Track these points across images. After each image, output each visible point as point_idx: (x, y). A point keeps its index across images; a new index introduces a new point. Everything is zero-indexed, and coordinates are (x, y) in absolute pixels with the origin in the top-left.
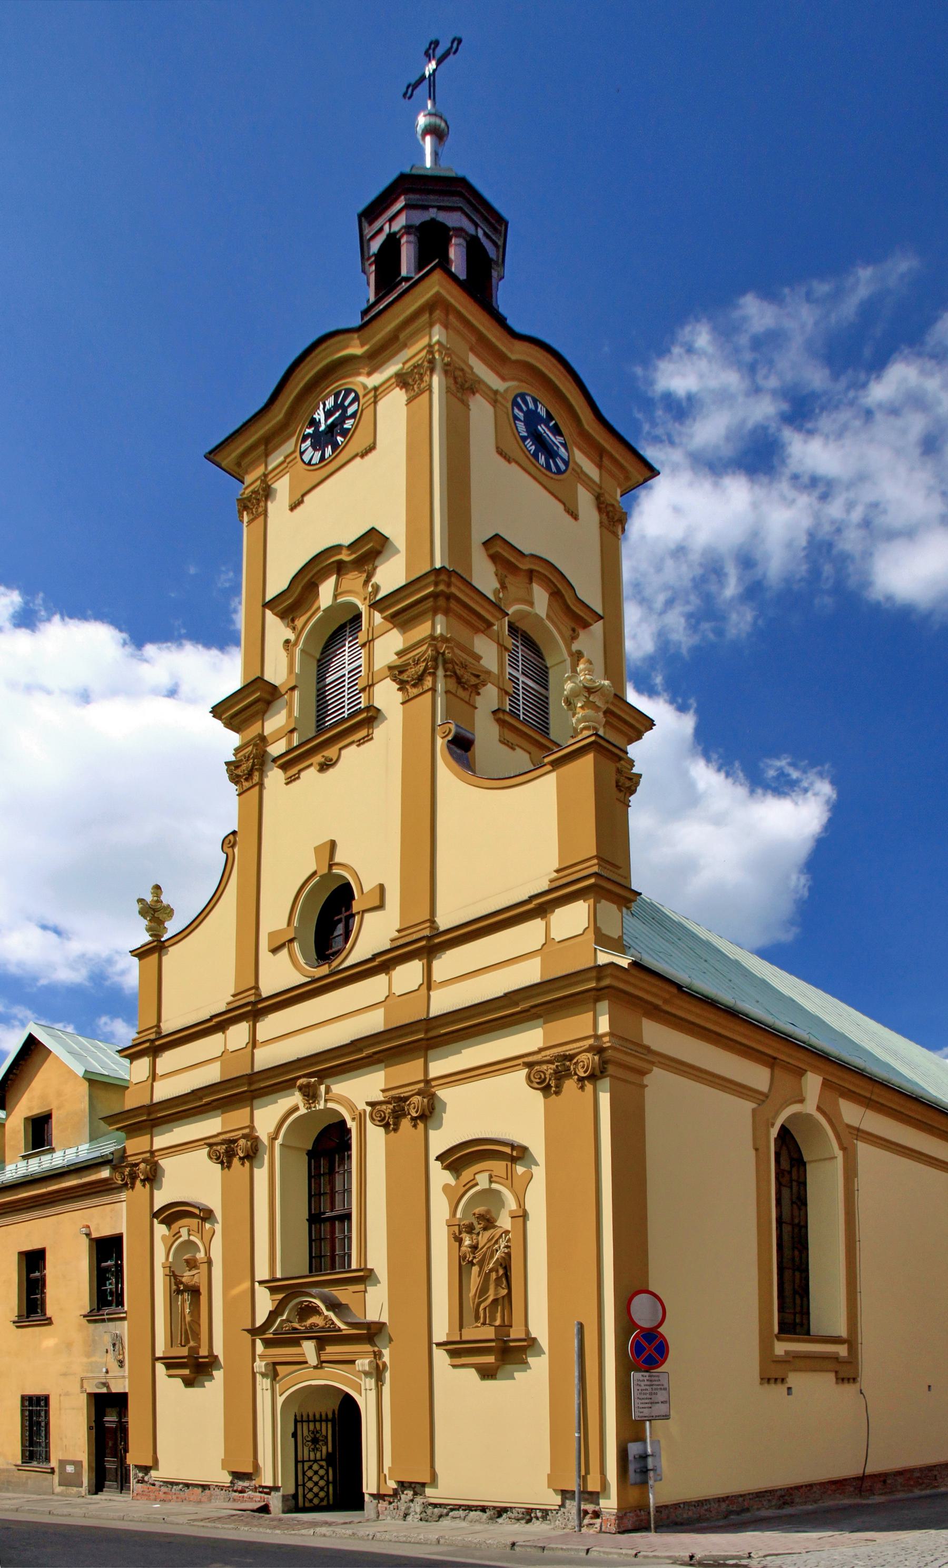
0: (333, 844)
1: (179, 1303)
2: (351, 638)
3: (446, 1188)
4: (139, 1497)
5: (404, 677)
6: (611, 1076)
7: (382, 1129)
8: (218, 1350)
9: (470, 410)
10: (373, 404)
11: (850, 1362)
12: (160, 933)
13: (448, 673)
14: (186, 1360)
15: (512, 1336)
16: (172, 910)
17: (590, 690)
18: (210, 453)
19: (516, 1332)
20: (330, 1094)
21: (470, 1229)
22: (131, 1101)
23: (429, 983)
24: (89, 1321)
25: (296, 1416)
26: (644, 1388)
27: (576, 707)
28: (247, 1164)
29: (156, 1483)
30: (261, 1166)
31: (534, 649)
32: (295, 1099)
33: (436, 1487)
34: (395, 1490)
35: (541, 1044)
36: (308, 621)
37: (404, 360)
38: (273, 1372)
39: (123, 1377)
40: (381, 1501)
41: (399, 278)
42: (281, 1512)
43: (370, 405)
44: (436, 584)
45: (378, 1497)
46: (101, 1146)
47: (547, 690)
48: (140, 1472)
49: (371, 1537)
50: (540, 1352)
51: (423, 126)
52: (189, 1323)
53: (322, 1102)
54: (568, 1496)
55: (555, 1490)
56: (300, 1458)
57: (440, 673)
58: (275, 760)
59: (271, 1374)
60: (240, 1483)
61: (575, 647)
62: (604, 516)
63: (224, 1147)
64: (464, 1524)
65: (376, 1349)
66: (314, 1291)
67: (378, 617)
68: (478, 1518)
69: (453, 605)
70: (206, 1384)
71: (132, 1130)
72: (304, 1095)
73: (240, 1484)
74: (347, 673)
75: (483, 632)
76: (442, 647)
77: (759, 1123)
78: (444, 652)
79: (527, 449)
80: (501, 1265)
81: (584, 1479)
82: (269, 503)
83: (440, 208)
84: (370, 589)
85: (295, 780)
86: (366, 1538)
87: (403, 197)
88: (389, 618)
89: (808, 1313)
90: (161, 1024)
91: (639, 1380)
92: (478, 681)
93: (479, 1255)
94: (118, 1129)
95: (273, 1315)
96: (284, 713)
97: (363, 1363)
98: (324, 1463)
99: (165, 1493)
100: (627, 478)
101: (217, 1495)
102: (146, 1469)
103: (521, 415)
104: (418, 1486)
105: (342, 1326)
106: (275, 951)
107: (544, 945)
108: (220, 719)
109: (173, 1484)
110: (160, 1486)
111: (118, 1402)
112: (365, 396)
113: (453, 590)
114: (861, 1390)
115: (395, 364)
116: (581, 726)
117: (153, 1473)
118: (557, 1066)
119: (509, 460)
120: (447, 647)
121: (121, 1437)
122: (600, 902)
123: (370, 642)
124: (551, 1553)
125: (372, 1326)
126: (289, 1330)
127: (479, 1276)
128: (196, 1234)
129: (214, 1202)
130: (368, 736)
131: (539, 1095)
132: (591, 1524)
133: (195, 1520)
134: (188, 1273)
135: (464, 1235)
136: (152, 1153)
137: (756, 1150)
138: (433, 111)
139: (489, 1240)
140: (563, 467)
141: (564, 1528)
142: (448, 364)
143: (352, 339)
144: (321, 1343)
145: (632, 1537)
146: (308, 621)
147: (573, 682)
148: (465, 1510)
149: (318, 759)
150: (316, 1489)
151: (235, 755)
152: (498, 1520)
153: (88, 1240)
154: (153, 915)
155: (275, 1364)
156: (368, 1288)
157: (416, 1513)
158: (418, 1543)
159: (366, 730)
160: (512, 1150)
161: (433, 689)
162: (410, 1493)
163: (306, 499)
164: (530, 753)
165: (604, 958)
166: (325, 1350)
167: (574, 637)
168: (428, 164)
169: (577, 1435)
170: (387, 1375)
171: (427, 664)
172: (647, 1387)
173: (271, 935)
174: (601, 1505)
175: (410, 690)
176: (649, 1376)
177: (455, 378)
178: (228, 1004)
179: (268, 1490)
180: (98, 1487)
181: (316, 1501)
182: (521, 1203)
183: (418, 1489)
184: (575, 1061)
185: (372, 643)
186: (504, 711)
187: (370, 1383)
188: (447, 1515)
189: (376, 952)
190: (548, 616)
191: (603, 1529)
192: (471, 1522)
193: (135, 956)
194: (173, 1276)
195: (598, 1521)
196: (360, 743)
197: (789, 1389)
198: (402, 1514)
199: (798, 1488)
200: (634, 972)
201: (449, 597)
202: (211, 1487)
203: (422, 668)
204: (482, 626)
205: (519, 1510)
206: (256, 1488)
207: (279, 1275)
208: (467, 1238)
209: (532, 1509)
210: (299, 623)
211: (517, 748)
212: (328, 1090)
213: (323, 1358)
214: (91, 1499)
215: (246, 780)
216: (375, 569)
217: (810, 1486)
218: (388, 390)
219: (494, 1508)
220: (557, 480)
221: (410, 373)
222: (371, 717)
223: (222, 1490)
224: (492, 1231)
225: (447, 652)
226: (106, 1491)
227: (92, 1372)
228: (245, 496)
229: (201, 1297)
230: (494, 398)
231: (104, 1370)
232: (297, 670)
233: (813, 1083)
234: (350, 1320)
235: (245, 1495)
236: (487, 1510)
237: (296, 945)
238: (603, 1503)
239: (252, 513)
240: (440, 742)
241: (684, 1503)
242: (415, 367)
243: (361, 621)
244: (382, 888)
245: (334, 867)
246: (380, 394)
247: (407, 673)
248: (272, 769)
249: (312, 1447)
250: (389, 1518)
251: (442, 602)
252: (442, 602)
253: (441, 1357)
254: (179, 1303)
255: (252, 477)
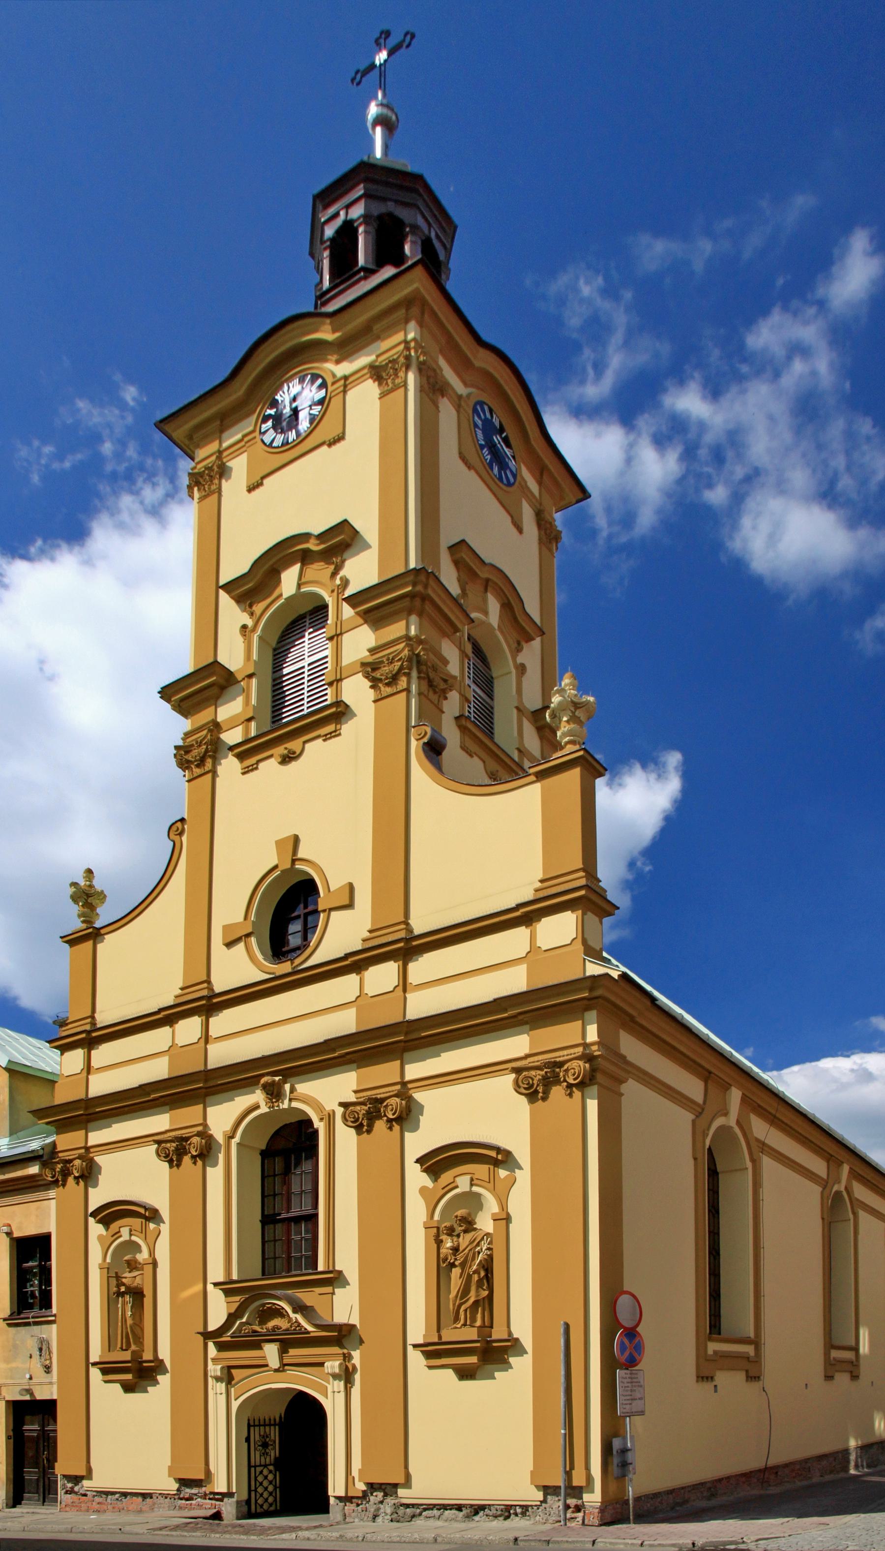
0: (296, 840)
1: (120, 1305)
2: (311, 630)
3: (423, 1191)
4: (68, 1509)
5: (377, 674)
6: (600, 1085)
7: (353, 1131)
8: (164, 1353)
9: (439, 412)
10: (342, 394)
11: (757, 1362)
12: (93, 920)
13: (422, 675)
14: (130, 1365)
15: (494, 1337)
16: (105, 896)
17: (576, 705)
18: (162, 421)
19: (498, 1333)
20: (295, 1094)
21: (450, 1232)
22: (62, 1096)
23: (404, 984)
24: (9, 1325)
25: (249, 1420)
26: (626, 1385)
27: (560, 721)
28: (200, 1163)
29: (87, 1493)
30: (215, 1164)
31: (482, 657)
32: (258, 1097)
33: (410, 1487)
34: (364, 1492)
35: (527, 1051)
36: (267, 608)
37: (379, 352)
38: (228, 1377)
39: (51, 1383)
40: (347, 1504)
41: (356, 269)
42: (235, 1518)
43: (338, 393)
44: (414, 584)
45: (346, 1499)
46: (22, 1142)
47: (492, 699)
48: (68, 1482)
49: (360, 1539)
50: (522, 1352)
51: (375, 116)
52: (131, 1327)
53: (286, 1102)
54: (549, 1491)
55: (537, 1487)
56: (253, 1463)
57: (414, 674)
58: (231, 748)
59: (225, 1377)
60: (188, 1490)
61: (520, 659)
62: (543, 533)
63: (174, 1145)
64: (439, 1523)
65: (345, 1351)
66: (279, 1292)
67: (348, 611)
68: (453, 1516)
69: (428, 607)
70: (149, 1389)
71: (63, 1126)
72: (267, 1094)
73: (188, 1491)
74: (306, 665)
75: (448, 637)
76: (417, 649)
77: (697, 1133)
78: (419, 653)
79: (484, 457)
80: (483, 1267)
81: (568, 1474)
82: (223, 481)
83: (397, 202)
84: (338, 582)
85: (252, 770)
86: (355, 1539)
87: (362, 186)
88: (362, 614)
89: (719, 1316)
90: (96, 1015)
91: (623, 1378)
92: (446, 686)
93: (460, 1258)
94: (48, 1123)
95: (232, 1318)
96: (240, 700)
97: (333, 1366)
98: (271, 1468)
99: (98, 1503)
100: (562, 498)
101: (161, 1504)
102: (77, 1479)
103: (479, 423)
104: (388, 1487)
105: (310, 1328)
106: (229, 945)
107: (528, 953)
108: (168, 701)
109: (107, 1493)
110: (94, 1496)
111: (48, 1408)
112: (333, 384)
113: (430, 592)
114: (763, 1388)
115: (369, 355)
116: (567, 739)
117: (86, 1483)
118: (546, 1072)
119: (470, 467)
120: (423, 649)
121: (44, 1446)
122: (586, 914)
123: (338, 635)
124: (556, 1546)
125: (344, 1328)
126: (248, 1332)
127: (460, 1278)
128: (140, 1234)
129: (161, 1202)
130: (335, 731)
131: (523, 1100)
132: (572, 1518)
133: (154, 1529)
134: (127, 1275)
135: (443, 1237)
136: (87, 1149)
137: (695, 1159)
138: (385, 102)
139: (471, 1243)
140: (512, 480)
141: (545, 1523)
142: (424, 363)
143: (324, 324)
144: (285, 1345)
145: (621, 1529)
146: (267, 608)
147: (561, 696)
148: (439, 1509)
149: (280, 750)
150: (266, 1495)
151: (183, 739)
152: (474, 1518)
153: (8, 1239)
154: (86, 900)
155: (230, 1368)
156: (336, 1290)
157: (387, 1514)
158: (413, 1542)
159: (334, 725)
160: (497, 1154)
161: (408, 690)
162: (380, 1495)
163: (265, 481)
164: (484, 762)
165: (594, 969)
166: (287, 1352)
167: (519, 649)
168: (378, 153)
169: (563, 1432)
170: (357, 1377)
171: (402, 664)
172: (629, 1385)
173: (226, 928)
174: (584, 1500)
175: (382, 688)
176: (631, 1374)
177: (428, 377)
178: (176, 997)
179: (220, 1497)
180: (16, 1499)
181: (265, 1507)
182: (503, 1206)
183: (388, 1488)
184: (565, 1067)
185: (340, 637)
186: (468, 718)
187: (340, 1385)
188: (420, 1514)
189: (348, 951)
190: (499, 626)
191: (586, 1522)
192: (446, 1521)
193: (66, 942)
194: (113, 1276)
195: (581, 1515)
196: (327, 737)
197: (716, 1386)
198: (371, 1516)
199: (720, 1480)
200: (623, 984)
201: (424, 598)
202: (153, 1495)
203: (396, 668)
204: (448, 629)
205: (498, 1507)
206: (205, 1494)
207: (235, 1277)
208: (449, 1240)
209: (512, 1505)
210: (258, 608)
211: (474, 755)
212: (293, 1090)
213: (285, 1361)
214: (10, 1512)
215: (198, 766)
216: (343, 562)
217: (728, 1478)
218: (359, 381)
219: (471, 1506)
220: (505, 491)
221: (383, 368)
222: (340, 712)
223: (166, 1498)
224: (473, 1233)
225: (422, 654)
226: (26, 1504)
227: (12, 1378)
228: (196, 471)
229: (145, 1300)
230: (458, 402)
231: (28, 1376)
232: (255, 656)
233: (735, 1095)
234: (318, 1322)
235: (193, 1502)
236: (463, 1509)
237: (253, 940)
238: (586, 1497)
239: (204, 489)
240: (414, 744)
241: (644, 1496)
242: (390, 362)
243: (328, 611)
244: (351, 887)
245: (297, 863)
246: (350, 383)
247: (380, 671)
248: (226, 757)
249: (263, 1451)
250: (356, 1520)
251: (418, 602)
252: (418, 602)
253: (416, 1359)
254: (120, 1305)
255: (206, 452)
